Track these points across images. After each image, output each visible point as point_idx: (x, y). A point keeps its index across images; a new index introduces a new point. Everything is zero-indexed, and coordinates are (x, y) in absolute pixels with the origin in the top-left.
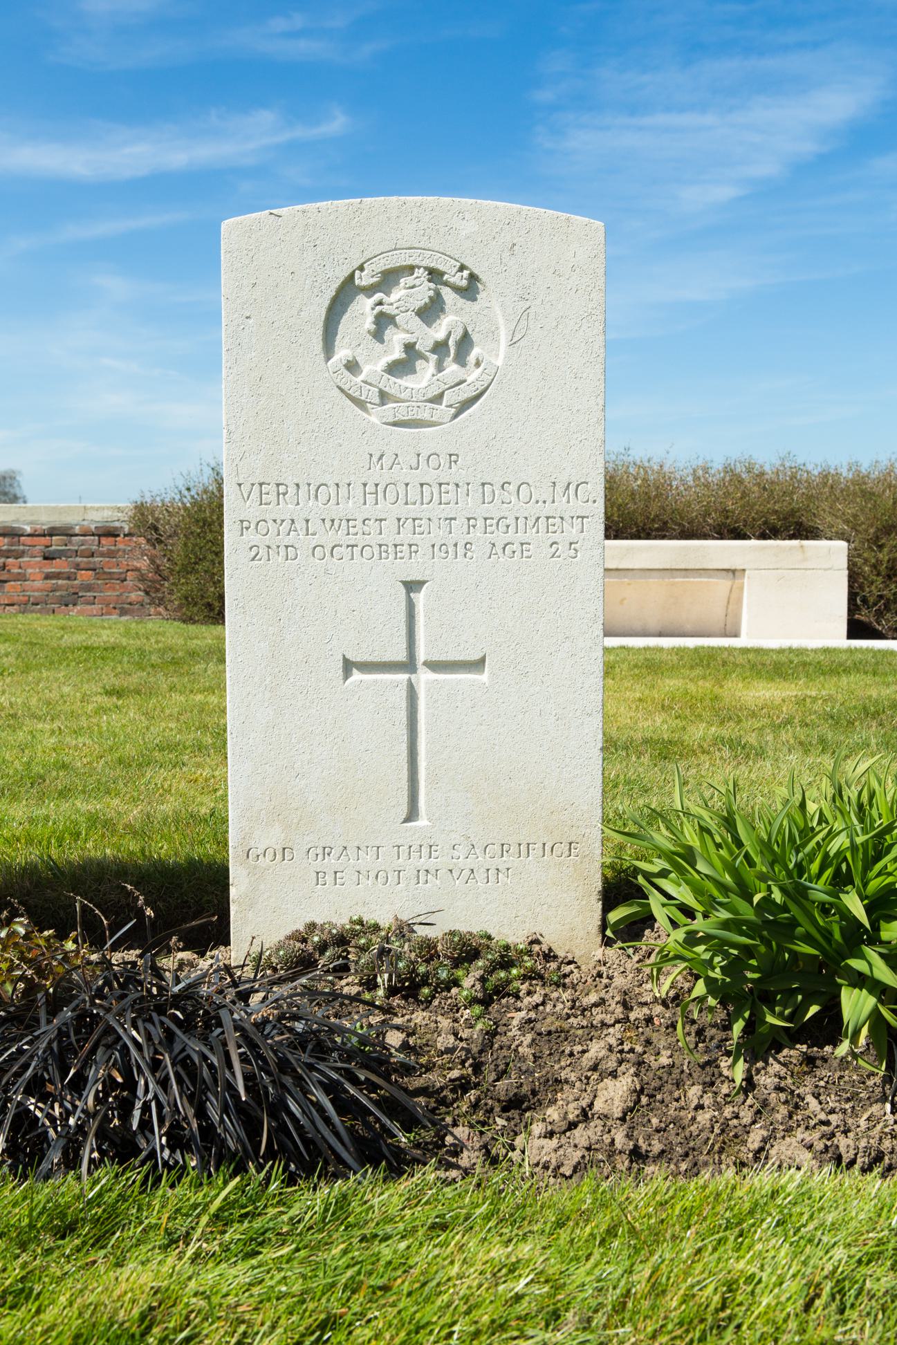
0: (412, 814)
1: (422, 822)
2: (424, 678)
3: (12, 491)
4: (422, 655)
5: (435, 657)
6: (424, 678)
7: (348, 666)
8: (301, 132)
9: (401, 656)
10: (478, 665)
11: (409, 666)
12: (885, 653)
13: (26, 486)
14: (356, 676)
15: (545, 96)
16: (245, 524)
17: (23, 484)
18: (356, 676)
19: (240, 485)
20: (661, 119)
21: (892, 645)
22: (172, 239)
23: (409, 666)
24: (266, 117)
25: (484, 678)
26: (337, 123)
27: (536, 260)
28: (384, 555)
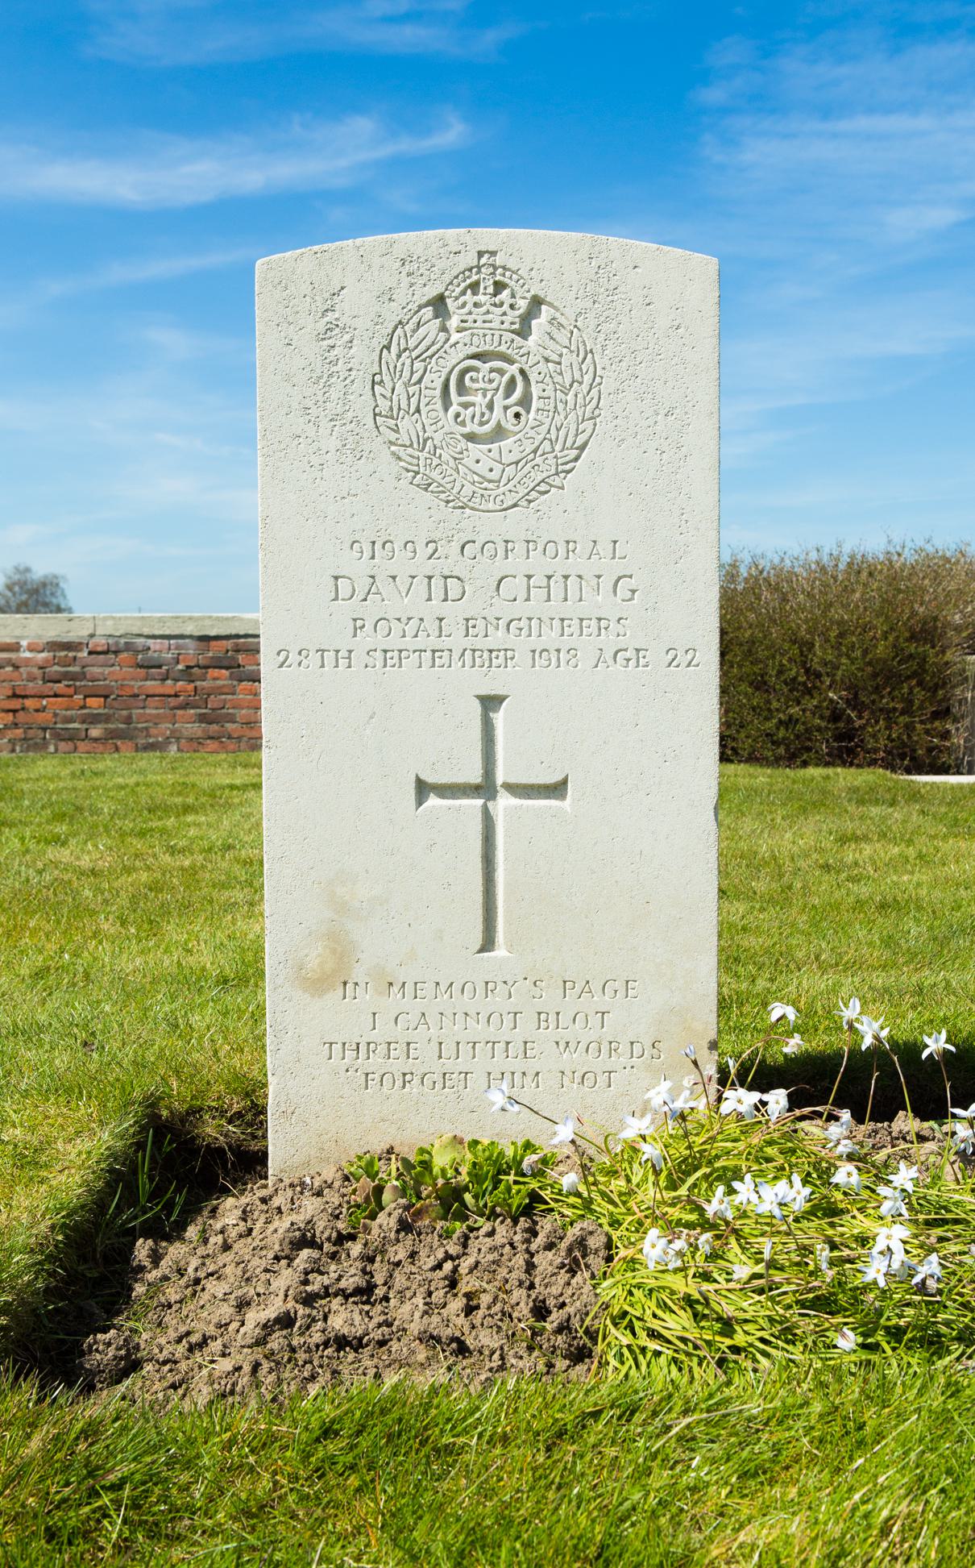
0: (488, 944)
1: (500, 952)
2: (504, 803)
3: (54, 601)
4: (500, 779)
5: (512, 780)
6: (504, 803)
7: (423, 789)
8: (406, 145)
9: (475, 776)
10: (557, 789)
11: (485, 789)
12: (961, 787)
13: (73, 595)
14: (433, 801)
15: (714, 95)
16: (359, 623)
17: (68, 593)
18: (433, 801)
19: (394, 578)
20: (863, 123)
21: (970, 779)
22: (202, 278)
23: (485, 789)
24: (363, 126)
25: (566, 804)
26: (452, 133)
27: (634, 293)
28: (478, 660)
